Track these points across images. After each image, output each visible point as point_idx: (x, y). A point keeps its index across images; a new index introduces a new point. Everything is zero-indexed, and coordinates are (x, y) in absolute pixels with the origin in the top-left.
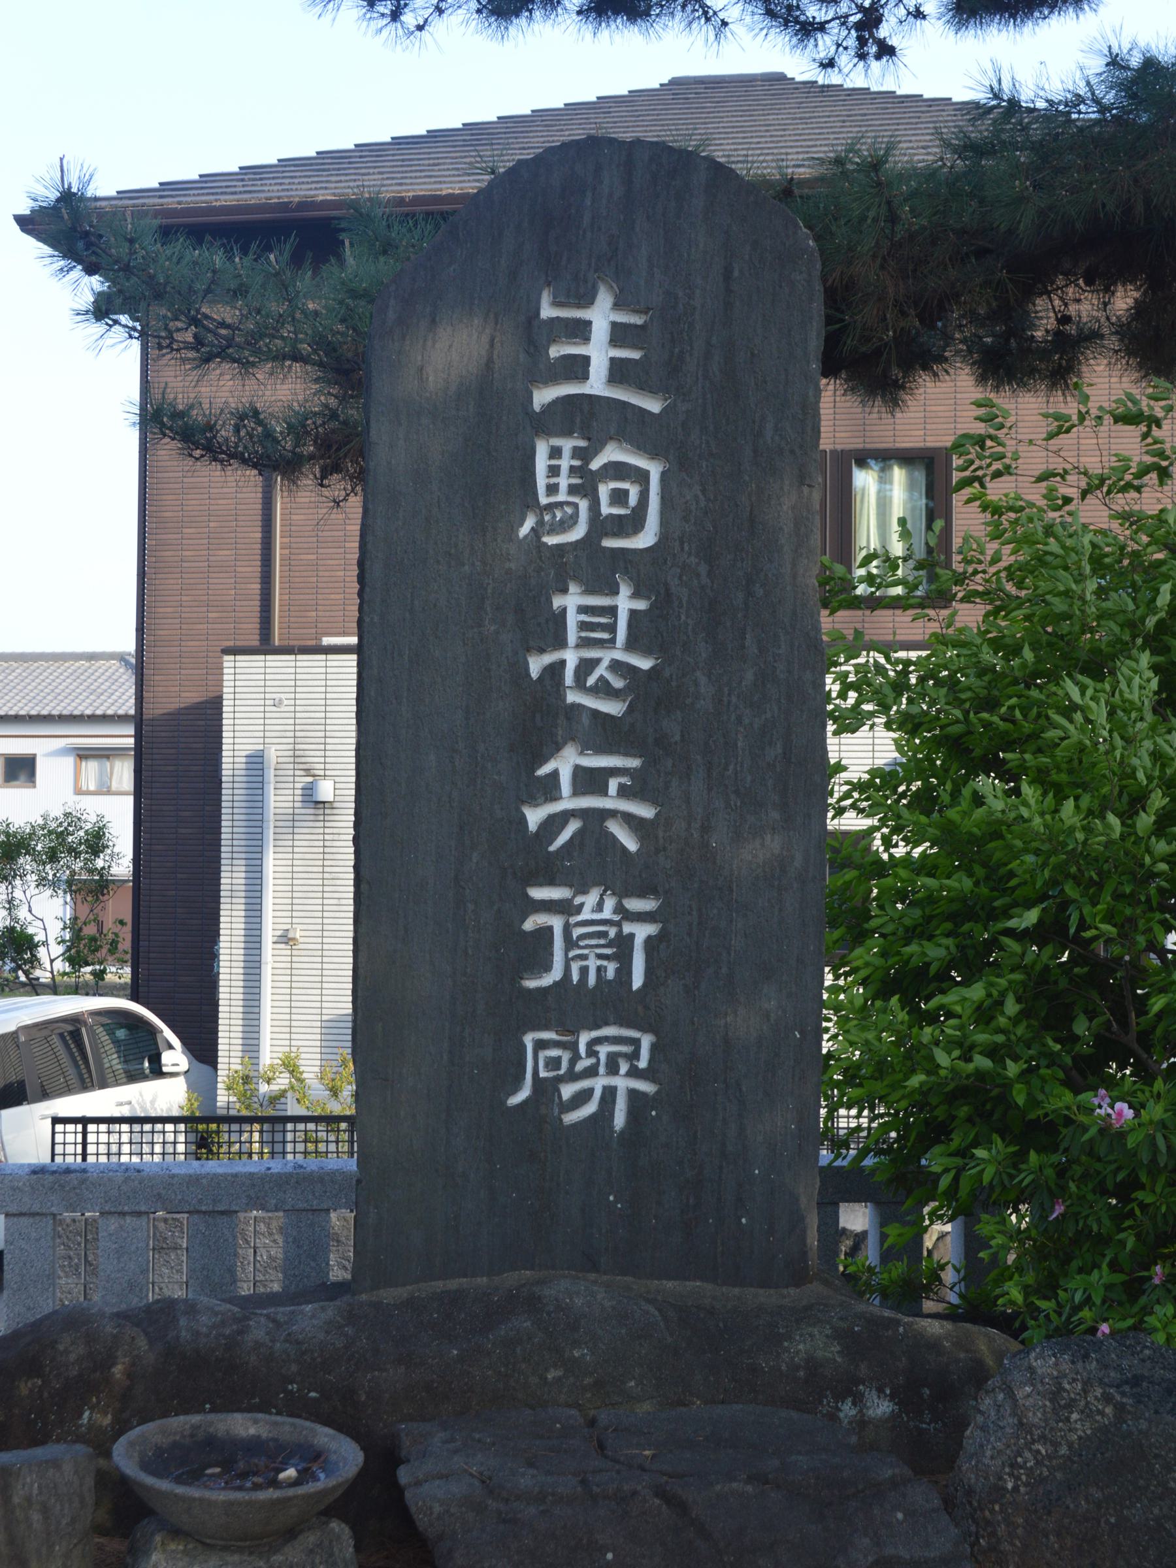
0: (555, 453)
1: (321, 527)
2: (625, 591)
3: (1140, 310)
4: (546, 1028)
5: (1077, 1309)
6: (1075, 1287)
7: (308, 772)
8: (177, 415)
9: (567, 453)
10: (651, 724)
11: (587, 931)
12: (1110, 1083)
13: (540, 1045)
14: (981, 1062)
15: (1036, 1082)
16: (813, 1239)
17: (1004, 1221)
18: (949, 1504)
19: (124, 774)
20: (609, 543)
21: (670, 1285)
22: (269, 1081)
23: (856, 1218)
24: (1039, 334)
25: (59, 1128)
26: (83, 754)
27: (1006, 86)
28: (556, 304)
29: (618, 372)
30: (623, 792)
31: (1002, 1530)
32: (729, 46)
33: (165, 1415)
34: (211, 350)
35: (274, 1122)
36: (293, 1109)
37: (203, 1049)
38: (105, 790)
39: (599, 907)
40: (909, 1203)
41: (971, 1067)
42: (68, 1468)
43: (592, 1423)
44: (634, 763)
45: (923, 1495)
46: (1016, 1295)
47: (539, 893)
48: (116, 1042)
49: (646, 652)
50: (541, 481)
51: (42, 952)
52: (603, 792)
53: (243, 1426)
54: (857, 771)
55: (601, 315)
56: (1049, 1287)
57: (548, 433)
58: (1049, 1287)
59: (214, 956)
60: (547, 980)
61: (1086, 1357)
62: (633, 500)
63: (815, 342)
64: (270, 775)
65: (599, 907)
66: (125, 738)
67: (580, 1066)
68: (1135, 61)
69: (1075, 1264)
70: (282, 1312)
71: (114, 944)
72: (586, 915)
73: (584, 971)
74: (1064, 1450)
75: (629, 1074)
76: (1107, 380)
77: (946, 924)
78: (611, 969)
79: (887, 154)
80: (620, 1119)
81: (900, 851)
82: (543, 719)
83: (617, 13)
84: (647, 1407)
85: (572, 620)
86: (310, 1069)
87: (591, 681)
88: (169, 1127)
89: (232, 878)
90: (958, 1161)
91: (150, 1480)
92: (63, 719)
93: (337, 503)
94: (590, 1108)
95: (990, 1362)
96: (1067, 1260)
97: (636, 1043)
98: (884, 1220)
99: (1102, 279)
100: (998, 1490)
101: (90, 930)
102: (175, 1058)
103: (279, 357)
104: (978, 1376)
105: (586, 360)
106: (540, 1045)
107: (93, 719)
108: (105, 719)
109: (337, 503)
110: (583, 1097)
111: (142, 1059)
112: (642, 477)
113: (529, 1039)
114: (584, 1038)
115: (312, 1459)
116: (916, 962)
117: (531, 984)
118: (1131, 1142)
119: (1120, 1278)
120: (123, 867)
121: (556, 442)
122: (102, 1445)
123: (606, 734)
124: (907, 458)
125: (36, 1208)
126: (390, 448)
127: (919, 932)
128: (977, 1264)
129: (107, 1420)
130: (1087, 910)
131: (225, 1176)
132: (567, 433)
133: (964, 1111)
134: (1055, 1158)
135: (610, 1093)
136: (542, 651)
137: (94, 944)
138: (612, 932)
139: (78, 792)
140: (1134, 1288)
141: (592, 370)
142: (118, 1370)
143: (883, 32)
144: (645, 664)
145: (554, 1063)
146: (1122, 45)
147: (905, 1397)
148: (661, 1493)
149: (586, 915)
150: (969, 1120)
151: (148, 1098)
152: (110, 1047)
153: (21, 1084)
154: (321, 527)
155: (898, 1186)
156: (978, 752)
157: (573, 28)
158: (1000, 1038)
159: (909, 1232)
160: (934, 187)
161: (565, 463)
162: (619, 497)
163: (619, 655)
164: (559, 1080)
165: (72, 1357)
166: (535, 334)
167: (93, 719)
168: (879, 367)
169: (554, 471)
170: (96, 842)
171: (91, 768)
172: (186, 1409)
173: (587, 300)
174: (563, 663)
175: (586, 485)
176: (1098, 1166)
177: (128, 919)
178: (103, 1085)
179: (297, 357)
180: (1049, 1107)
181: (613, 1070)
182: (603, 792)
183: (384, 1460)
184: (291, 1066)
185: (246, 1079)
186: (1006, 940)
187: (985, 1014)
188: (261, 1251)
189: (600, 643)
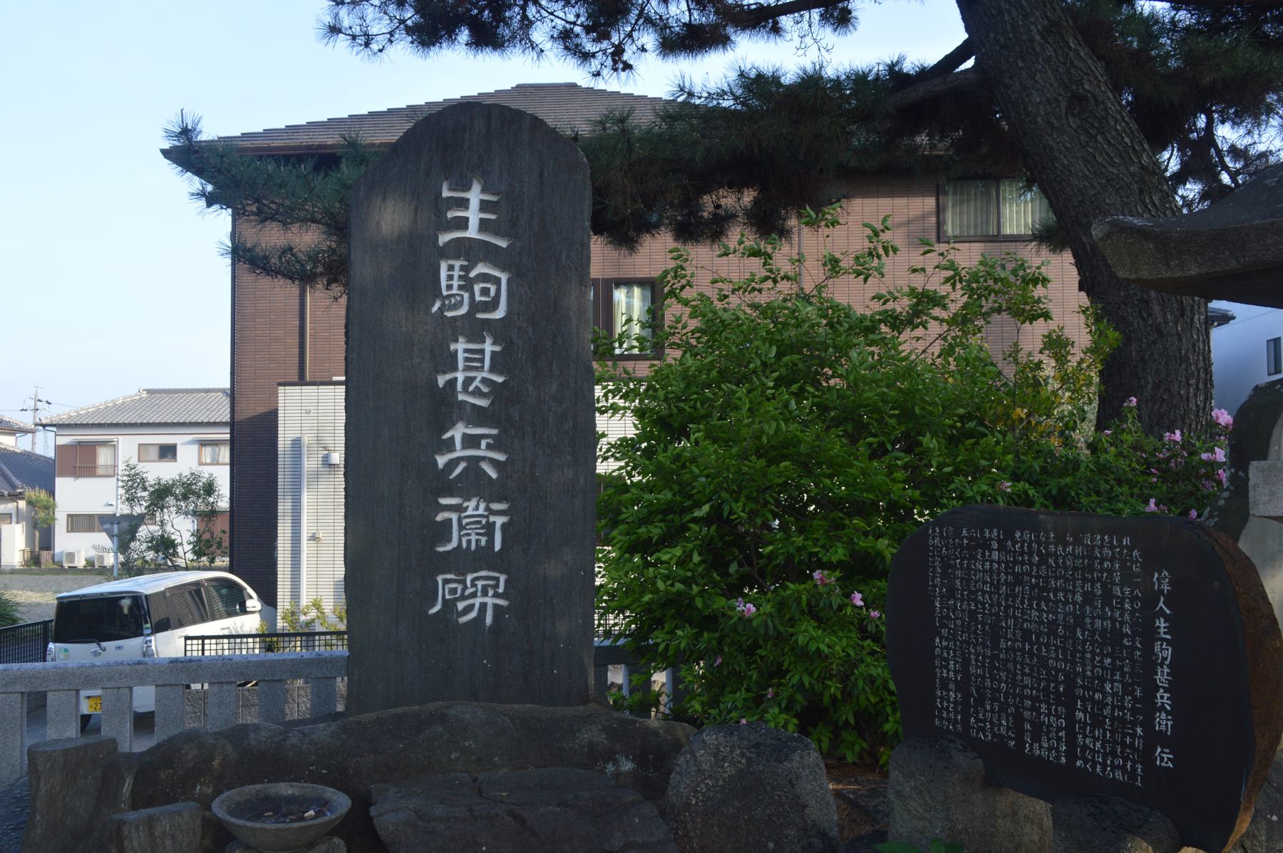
0: (451, 268)
1: (327, 310)
2: (489, 341)
3: (756, 202)
4: (449, 572)
5: (729, 712)
6: (728, 700)
7: (325, 448)
9: (457, 268)
10: (504, 411)
11: (470, 520)
12: (744, 596)
13: (446, 582)
14: (679, 586)
15: (706, 596)
16: (591, 681)
17: (691, 669)
18: (662, 814)
19: (225, 454)
20: (480, 316)
21: (516, 706)
22: (305, 614)
23: (617, 676)
24: (705, 214)
25: (189, 642)
26: (203, 443)
27: (687, 85)
28: (451, 189)
29: (484, 225)
30: (489, 447)
31: (690, 826)
32: (544, 62)
33: (242, 785)
34: (264, 217)
35: (308, 635)
36: (319, 628)
37: (269, 598)
38: (215, 462)
39: (477, 508)
40: (642, 662)
41: (675, 589)
43: (475, 780)
44: (494, 432)
46: (698, 707)
47: (444, 501)
48: (221, 596)
49: (500, 373)
50: (444, 283)
51: (180, 549)
52: (478, 447)
53: (285, 789)
54: (613, 438)
55: (475, 196)
56: (714, 703)
57: (447, 258)
58: (714, 703)
59: (275, 548)
60: (449, 547)
61: (732, 734)
62: (492, 293)
63: (587, 212)
64: (305, 450)
65: (477, 508)
66: (225, 434)
68: (753, 74)
69: (728, 689)
70: (306, 729)
71: (219, 545)
72: (469, 512)
73: (469, 542)
74: (721, 782)
75: (494, 596)
77: (658, 513)
78: (483, 540)
79: (629, 115)
80: (489, 620)
81: (637, 479)
82: (445, 408)
83: (487, 46)
84: (505, 770)
85: (461, 356)
86: (328, 607)
87: (471, 389)
88: (250, 640)
89: (284, 506)
90: (669, 636)
91: (233, 820)
92: (192, 424)
93: (336, 299)
94: (473, 615)
95: (683, 740)
96: (723, 688)
97: (497, 579)
98: (631, 672)
99: (737, 185)
100: (687, 805)
101: (206, 536)
102: (254, 603)
103: (304, 221)
104: (677, 747)
105: (467, 219)
106: (446, 582)
107: (209, 424)
108: (215, 424)
109: (336, 299)
110: (469, 609)
111: (235, 604)
112: (497, 281)
113: (440, 579)
114: (469, 578)
115: (323, 805)
116: (644, 536)
117: (441, 549)
118: (755, 624)
119: (752, 695)
120: (224, 504)
121: (451, 262)
122: (206, 803)
123: (479, 416)
124: (641, 283)
126: (363, 268)
127: (645, 520)
128: (679, 692)
129: (210, 790)
130: (734, 505)
132: (457, 258)
134: (717, 635)
135: (483, 606)
136: (445, 373)
137: (208, 544)
138: (484, 521)
139: (201, 464)
140: (758, 700)
141: (470, 224)
142: (216, 763)
143: (625, 57)
144: (500, 379)
145: (453, 591)
146: (747, 66)
148: (511, 814)
149: (469, 512)
150: (673, 617)
151: (239, 625)
153: (168, 619)
154: (327, 310)
155: (638, 654)
156: (676, 425)
157: (463, 53)
158: (689, 574)
159: (643, 677)
160: (652, 139)
161: (456, 273)
162: (485, 292)
164: (457, 600)
165: (190, 757)
166: (440, 206)
167: (209, 424)
168: (625, 234)
169: (450, 278)
170: (210, 489)
171: (208, 451)
172: (253, 782)
173: (467, 187)
174: (456, 379)
175: (467, 285)
176: (738, 638)
177: (227, 530)
178: (214, 619)
179: (314, 221)
180: (715, 607)
181: (485, 594)
182: (478, 447)
183: (362, 804)
184: (317, 605)
185: (293, 613)
186: (692, 525)
187: (682, 562)
188: (300, 700)
189: (476, 369)
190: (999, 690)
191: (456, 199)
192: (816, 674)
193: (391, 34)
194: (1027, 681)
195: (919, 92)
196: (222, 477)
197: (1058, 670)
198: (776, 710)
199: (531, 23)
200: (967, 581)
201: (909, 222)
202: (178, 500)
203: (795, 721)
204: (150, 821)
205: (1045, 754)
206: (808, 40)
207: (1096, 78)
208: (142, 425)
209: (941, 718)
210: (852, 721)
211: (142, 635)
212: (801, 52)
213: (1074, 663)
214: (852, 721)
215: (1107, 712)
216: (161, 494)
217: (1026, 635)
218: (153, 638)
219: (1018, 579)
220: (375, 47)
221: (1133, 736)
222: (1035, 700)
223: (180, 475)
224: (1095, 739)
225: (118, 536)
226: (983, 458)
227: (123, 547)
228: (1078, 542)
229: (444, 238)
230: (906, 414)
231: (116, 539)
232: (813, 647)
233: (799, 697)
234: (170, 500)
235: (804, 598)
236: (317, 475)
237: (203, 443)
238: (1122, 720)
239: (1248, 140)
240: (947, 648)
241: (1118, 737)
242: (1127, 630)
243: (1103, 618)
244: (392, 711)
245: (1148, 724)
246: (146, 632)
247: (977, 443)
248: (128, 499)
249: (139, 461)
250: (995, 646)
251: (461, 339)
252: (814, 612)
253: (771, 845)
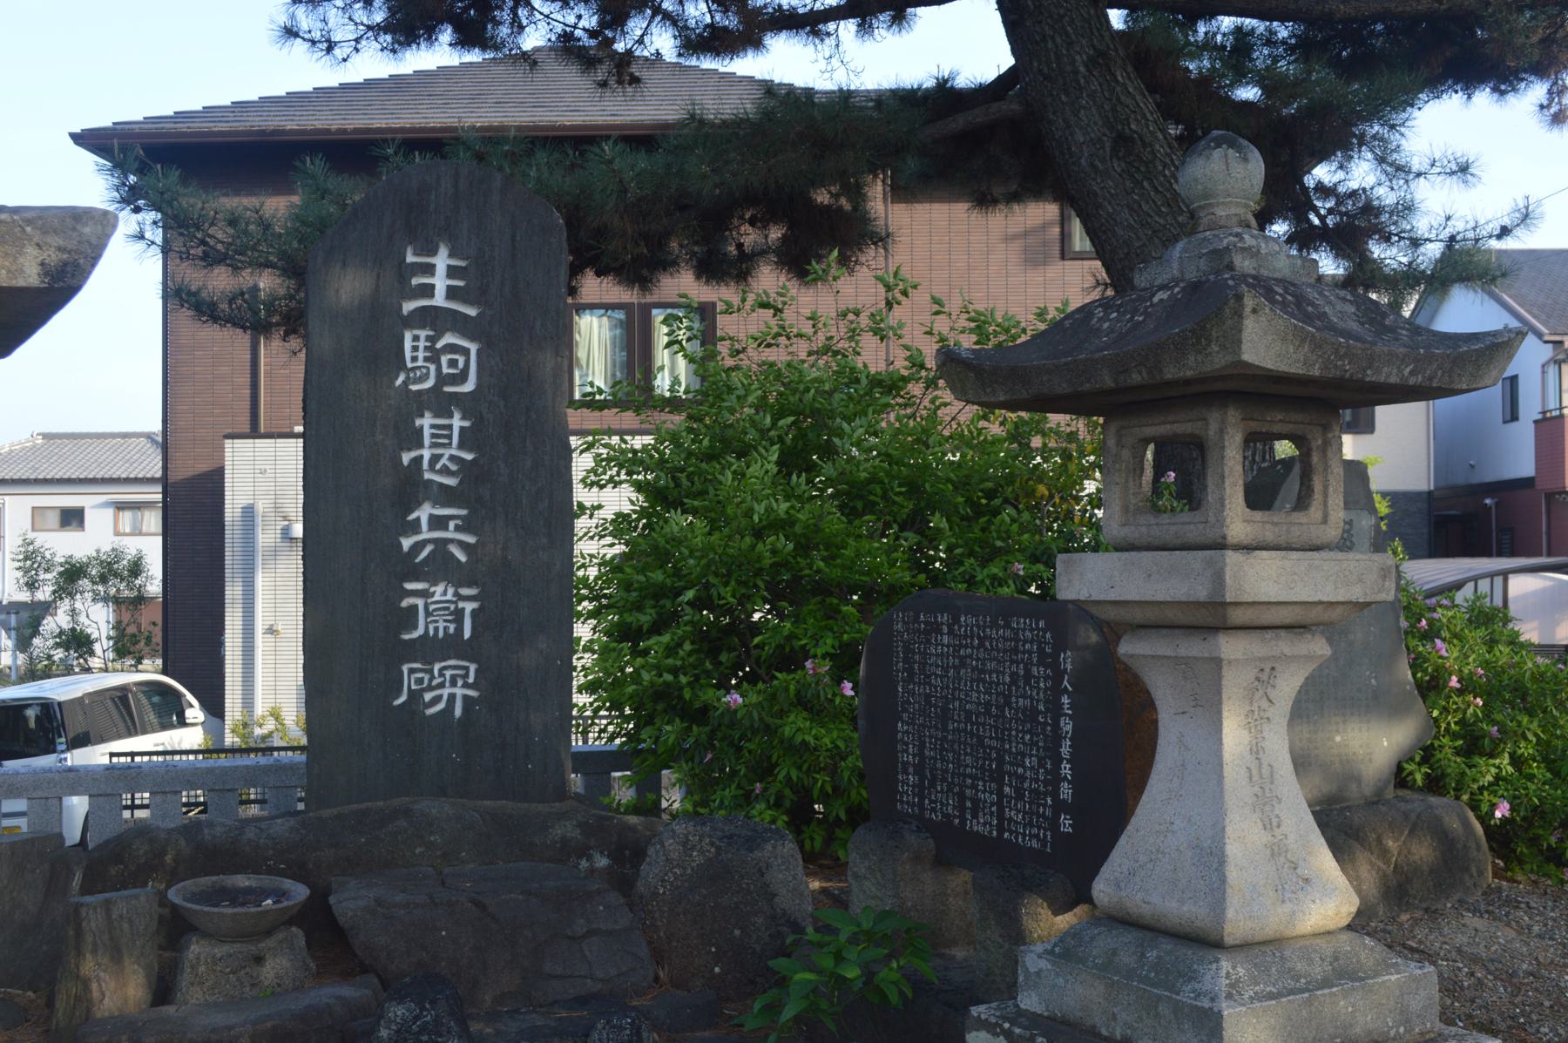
0: (416, 338)
1: (283, 367)
2: (457, 416)
4: (415, 661)
7: (285, 518)
8: (190, 293)
9: (422, 338)
10: (475, 490)
11: (437, 606)
13: (412, 671)
14: (668, 677)
19: (153, 521)
20: (448, 389)
22: (260, 726)
26: (120, 507)
28: (415, 254)
29: (452, 293)
30: (458, 529)
34: (211, 259)
36: (277, 743)
37: (214, 706)
38: (137, 532)
39: (445, 593)
42: (142, 899)
44: (464, 512)
45: (614, 898)
47: (409, 586)
48: (153, 705)
49: (470, 450)
50: (408, 354)
51: (97, 648)
52: (446, 529)
53: (242, 881)
55: (441, 261)
57: (412, 328)
60: (415, 635)
64: (259, 520)
65: (445, 593)
66: (155, 494)
67: (435, 683)
71: (149, 640)
72: (436, 598)
73: (436, 629)
76: (768, 279)
80: (458, 712)
82: (411, 488)
85: (427, 432)
87: (438, 467)
89: (233, 591)
97: (467, 669)
101: (131, 630)
102: (195, 713)
105: (433, 286)
106: (412, 671)
110: (437, 699)
111: (170, 712)
112: (465, 352)
113: (405, 668)
114: (437, 667)
117: (406, 637)
118: (739, 715)
119: (740, 792)
120: (154, 587)
121: (416, 332)
123: (446, 496)
125: (109, 791)
130: (722, 590)
131: (230, 768)
132: (423, 327)
133: (660, 707)
134: (707, 729)
135: (452, 697)
136: (409, 450)
137: (134, 639)
138: (452, 607)
139: (117, 533)
142: (168, 858)
144: (469, 457)
145: (420, 681)
147: (616, 856)
148: (473, 901)
150: (665, 711)
151: (176, 741)
152: (148, 708)
154: (283, 367)
158: (679, 663)
163: (454, 452)
164: (423, 690)
166: (404, 272)
169: (415, 349)
170: (136, 568)
171: (127, 517)
175: (434, 357)
178: (144, 732)
182: (446, 529)
184: (276, 715)
187: (671, 650)
190: (946, 771)
191: (421, 265)
192: (805, 767)
193: (357, 40)
194: (969, 760)
195: (977, 116)
196: (151, 550)
197: (991, 748)
198: (763, 806)
199: (522, 28)
200: (923, 665)
201: (1026, 234)
202: (94, 583)
203: (785, 818)
204: (108, 903)
205: (981, 829)
206: (835, 62)
207: (1144, 116)
208: (37, 482)
209: (902, 802)
210: (843, 816)
211: (54, 751)
212: (827, 75)
213: (1003, 741)
214: (843, 816)
215: (1026, 785)
216: (72, 574)
217: (969, 713)
218: (68, 755)
219: (963, 665)
220: (338, 52)
221: (1045, 806)
222: (974, 777)
223: (98, 551)
224: (1018, 811)
225: (17, 629)
226: (999, 538)
227: (23, 644)
228: (1007, 626)
229: (408, 307)
230: (913, 489)
231: (13, 633)
232: (798, 739)
233: (787, 792)
234: (84, 583)
235: (792, 687)
236: (275, 552)
237: (120, 507)
238: (1036, 791)
239: (1335, 179)
240: (907, 732)
241: (1034, 807)
242: (1041, 708)
243: (1025, 697)
244: (355, 807)
245: (1055, 794)
246: (60, 748)
247: (990, 522)
248: (27, 584)
249: (33, 530)
250: (945, 729)
251: (427, 414)
252: (803, 702)
253: (737, 932)
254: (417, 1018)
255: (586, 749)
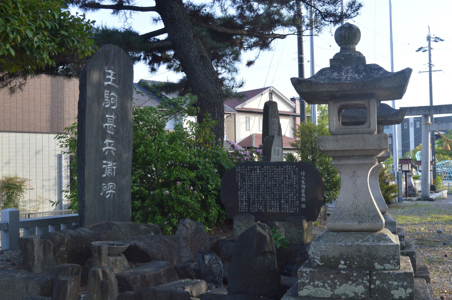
30: (113, 146)
82: (104, 134)
229: (106, 83)
254: (212, 258)
255: (29, 220)
